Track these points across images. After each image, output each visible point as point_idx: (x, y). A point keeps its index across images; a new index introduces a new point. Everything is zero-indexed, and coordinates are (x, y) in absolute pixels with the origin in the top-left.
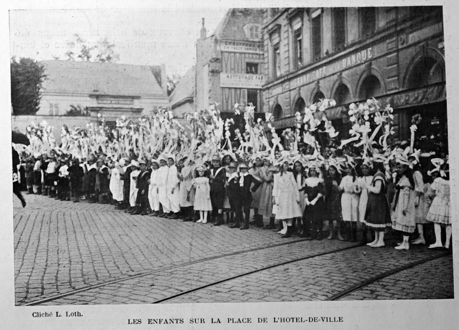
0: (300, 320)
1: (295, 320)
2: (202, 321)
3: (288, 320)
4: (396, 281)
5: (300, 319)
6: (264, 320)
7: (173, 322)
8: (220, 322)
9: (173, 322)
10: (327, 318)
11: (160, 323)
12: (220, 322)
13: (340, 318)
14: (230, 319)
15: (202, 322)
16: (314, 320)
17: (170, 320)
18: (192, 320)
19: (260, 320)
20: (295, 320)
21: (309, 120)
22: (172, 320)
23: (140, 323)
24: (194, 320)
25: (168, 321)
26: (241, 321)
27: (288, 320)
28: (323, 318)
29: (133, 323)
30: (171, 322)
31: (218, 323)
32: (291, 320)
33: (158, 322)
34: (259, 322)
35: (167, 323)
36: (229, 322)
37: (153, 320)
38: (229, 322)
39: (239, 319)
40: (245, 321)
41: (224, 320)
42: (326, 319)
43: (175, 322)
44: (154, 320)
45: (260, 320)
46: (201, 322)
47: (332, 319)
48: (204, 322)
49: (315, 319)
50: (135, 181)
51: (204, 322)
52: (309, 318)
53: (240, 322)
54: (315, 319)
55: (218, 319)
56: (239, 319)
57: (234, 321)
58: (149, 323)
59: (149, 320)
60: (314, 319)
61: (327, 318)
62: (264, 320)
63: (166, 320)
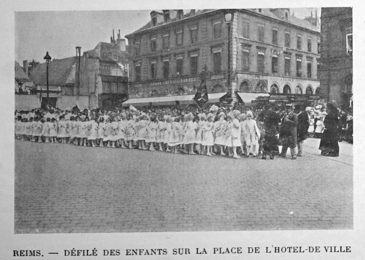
0: (298, 250)
1: (292, 250)
2: (239, 250)
3: (284, 250)
4: (38, 222)
5: (299, 249)
6: (256, 250)
7: (155, 253)
8: (206, 253)
9: (155, 253)
10: (331, 247)
11: (140, 254)
12: (206, 253)
13: (347, 247)
14: (216, 250)
15: (187, 252)
16: (315, 250)
17: (152, 250)
18: (175, 250)
19: (67, 253)
20: (292, 250)
21: (47, 53)
22: (154, 251)
23: (118, 254)
24: (178, 251)
25: (150, 252)
26: (230, 251)
27: (284, 250)
28: (327, 248)
29: (346, 251)
30: (153, 253)
31: (204, 254)
32: (288, 250)
33: (138, 252)
34: (65, 255)
35: (148, 254)
36: (215, 253)
37: (132, 251)
38: (215, 253)
39: (227, 249)
40: (234, 251)
41: (210, 251)
42: (330, 248)
43: (157, 252)
44: (133, 250)
45: (67, 253)
46: (186, 253)
47: (338, 249)
48: (189, 253)
49: (317, 249)
50: (199, 22)
51: (189, 253)
52: (310, 247)
53: (229, 253)
54: (317, 249)
55: (204, 249)
56: (227, 249)
57: (222, 252)
58: (127, 254)
59: (127, 250)
60: (71, 252)
61: (331, 247)
62: (256, 250)
63: (147, 251)
